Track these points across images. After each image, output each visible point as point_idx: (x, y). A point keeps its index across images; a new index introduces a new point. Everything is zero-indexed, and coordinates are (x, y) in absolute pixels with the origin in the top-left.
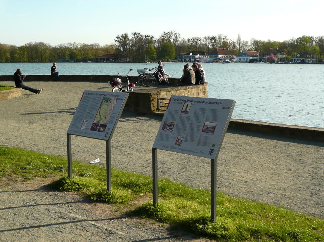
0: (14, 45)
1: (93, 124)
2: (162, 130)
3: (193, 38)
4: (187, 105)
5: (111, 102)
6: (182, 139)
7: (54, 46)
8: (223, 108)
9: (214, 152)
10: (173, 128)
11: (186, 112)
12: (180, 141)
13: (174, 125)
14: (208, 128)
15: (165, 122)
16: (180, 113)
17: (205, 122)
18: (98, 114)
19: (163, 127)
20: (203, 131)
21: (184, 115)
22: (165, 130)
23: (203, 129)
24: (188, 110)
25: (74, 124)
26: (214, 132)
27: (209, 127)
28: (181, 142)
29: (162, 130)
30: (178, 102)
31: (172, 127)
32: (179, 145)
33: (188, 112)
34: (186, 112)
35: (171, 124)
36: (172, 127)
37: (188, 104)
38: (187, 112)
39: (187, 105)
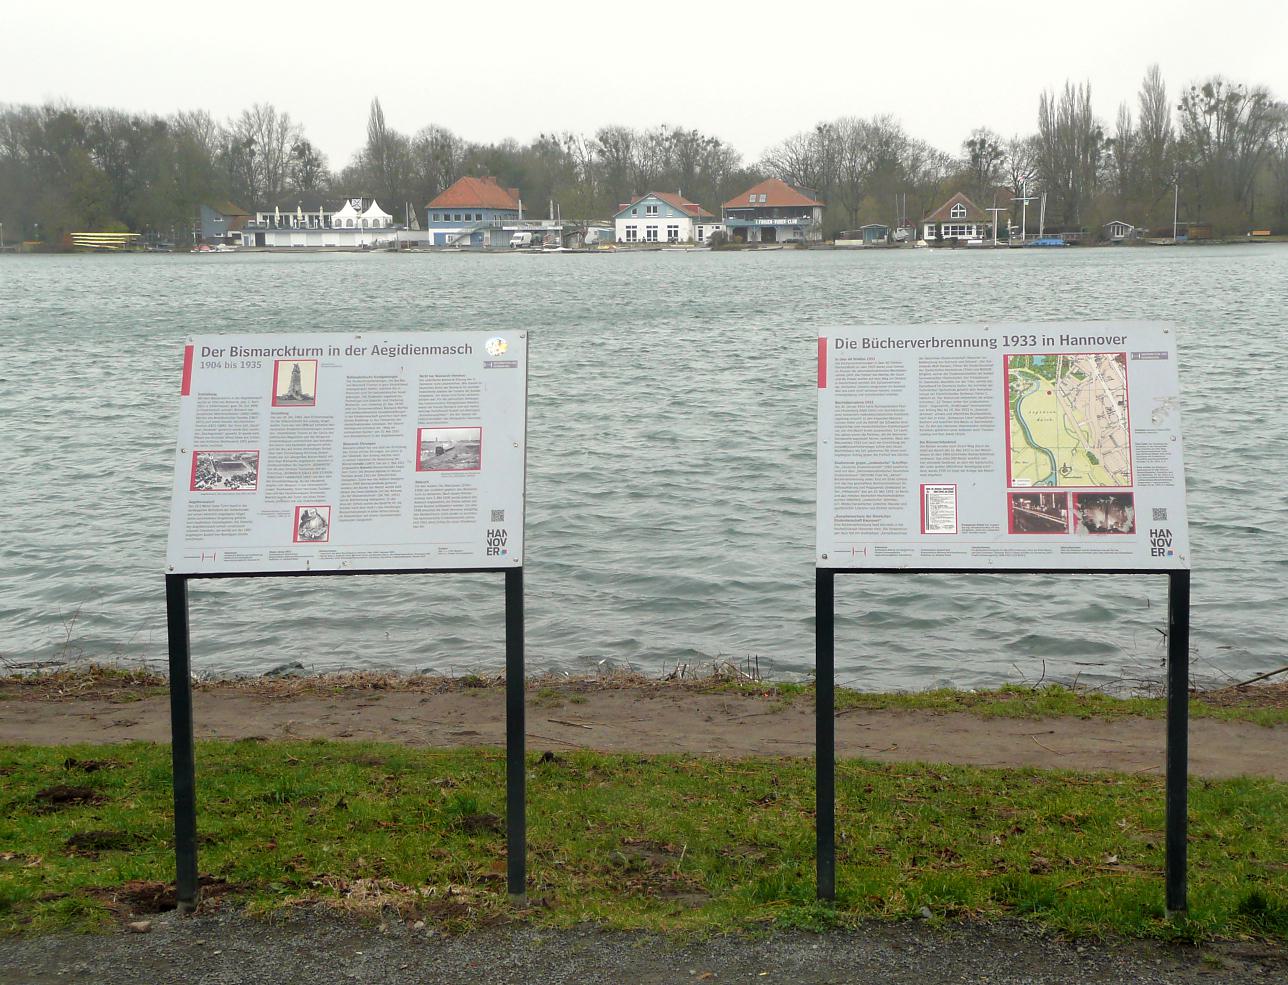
0: (496, 145)
1: (1014, 497)
2: (193, 488)
3: (200, 112)
4: (296, 371)
5: (1080, 375)
6: (324, 512)
7: (366, 146)
8: (487, 367)
9: (1175, 537)
10: (254, 477)
11: (296, 397)
12: (314, 523)
13: (254, 463)
14: (440, 451)
15: (196, 454)
16: (265, 406)
17: (419, 431)
18: (1018, 440)
19: (194, 477)
20: (420, 467)
21: (293, 411)
22: (209, 489)
23: (422, 459)
24: (307, 388)
25: (842, 513)
26: (478, 462)
27: (446, 446)
28: (324, 523)
29: (193, 488)
30: (237, 359)
31: (249, 469)
32: (316, 539)
33: (313, 399)
34: (296, 397)
35: (237, 458)
36: (249, 469)
37: (296, 366)
38: (308, 400)
39: (296, 371)
